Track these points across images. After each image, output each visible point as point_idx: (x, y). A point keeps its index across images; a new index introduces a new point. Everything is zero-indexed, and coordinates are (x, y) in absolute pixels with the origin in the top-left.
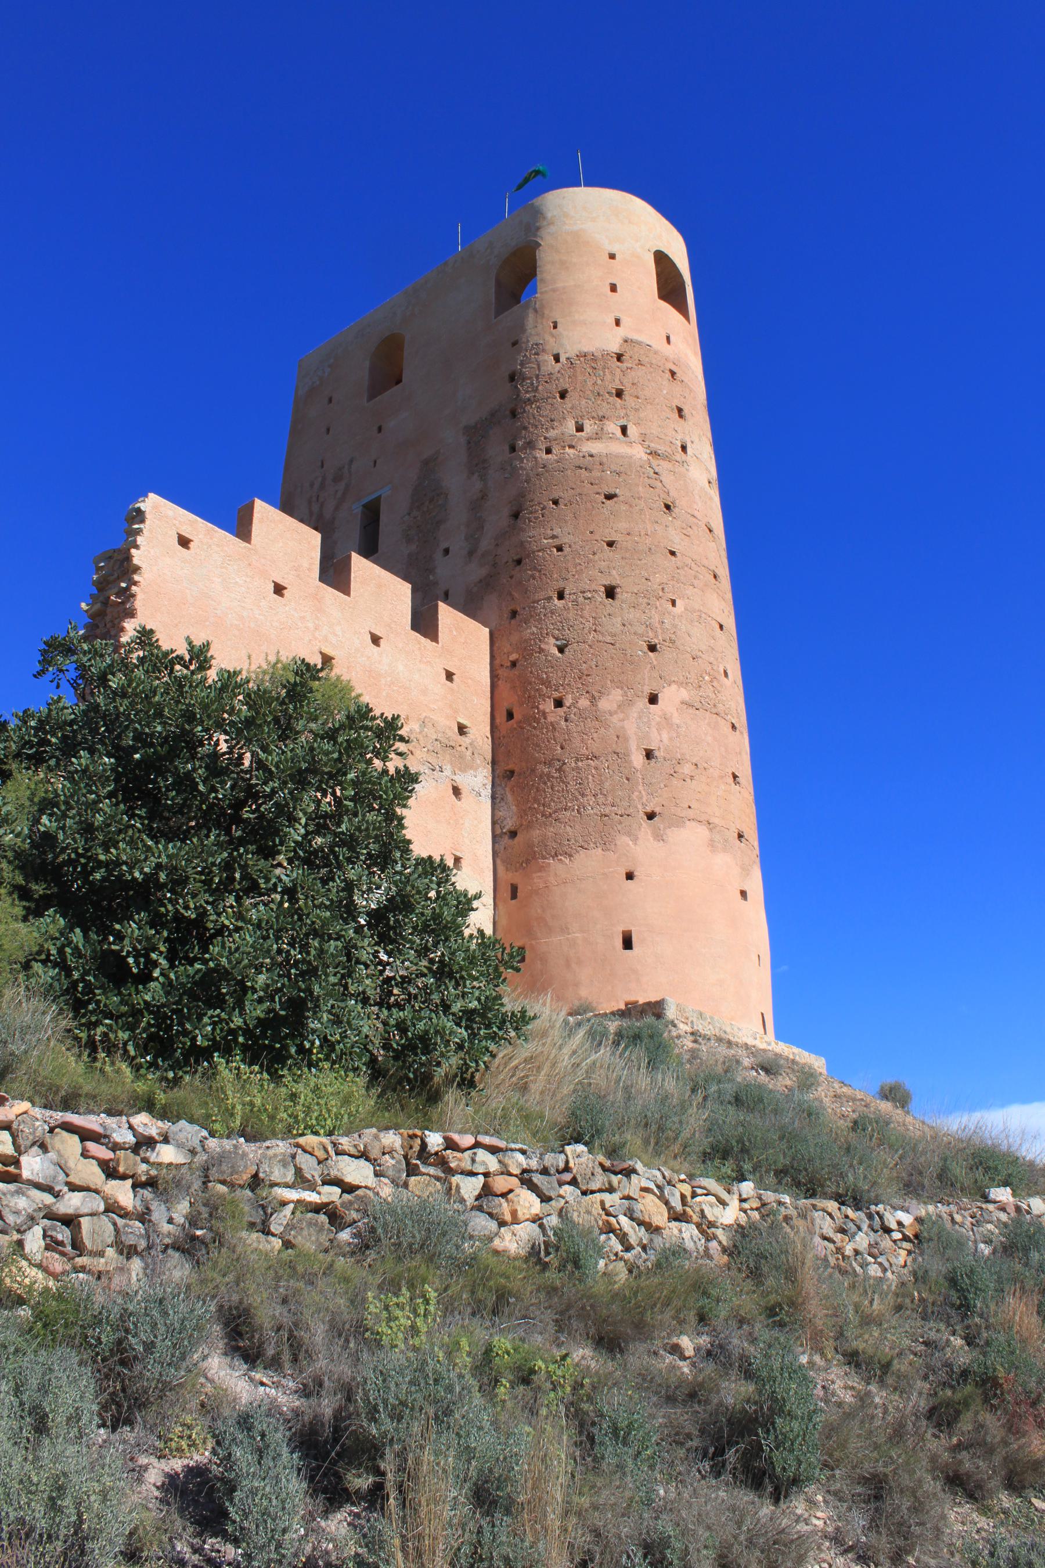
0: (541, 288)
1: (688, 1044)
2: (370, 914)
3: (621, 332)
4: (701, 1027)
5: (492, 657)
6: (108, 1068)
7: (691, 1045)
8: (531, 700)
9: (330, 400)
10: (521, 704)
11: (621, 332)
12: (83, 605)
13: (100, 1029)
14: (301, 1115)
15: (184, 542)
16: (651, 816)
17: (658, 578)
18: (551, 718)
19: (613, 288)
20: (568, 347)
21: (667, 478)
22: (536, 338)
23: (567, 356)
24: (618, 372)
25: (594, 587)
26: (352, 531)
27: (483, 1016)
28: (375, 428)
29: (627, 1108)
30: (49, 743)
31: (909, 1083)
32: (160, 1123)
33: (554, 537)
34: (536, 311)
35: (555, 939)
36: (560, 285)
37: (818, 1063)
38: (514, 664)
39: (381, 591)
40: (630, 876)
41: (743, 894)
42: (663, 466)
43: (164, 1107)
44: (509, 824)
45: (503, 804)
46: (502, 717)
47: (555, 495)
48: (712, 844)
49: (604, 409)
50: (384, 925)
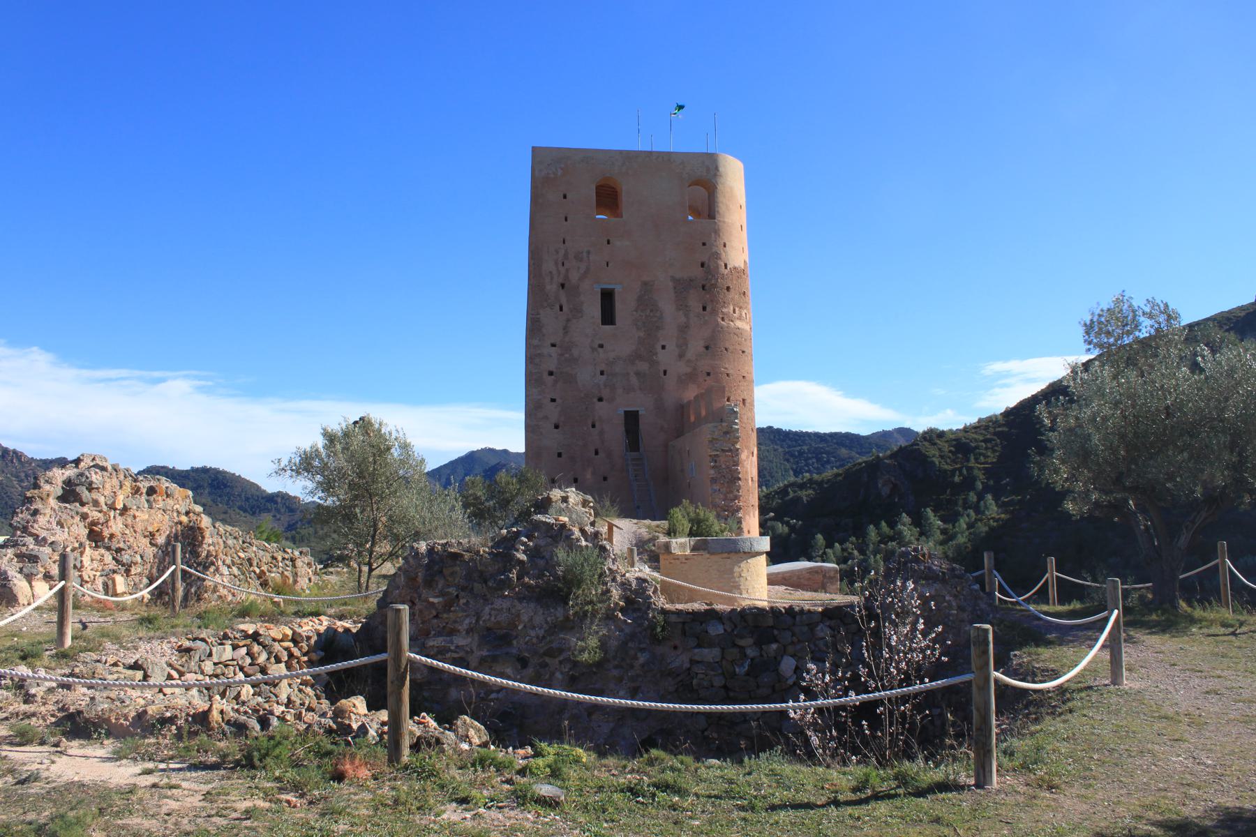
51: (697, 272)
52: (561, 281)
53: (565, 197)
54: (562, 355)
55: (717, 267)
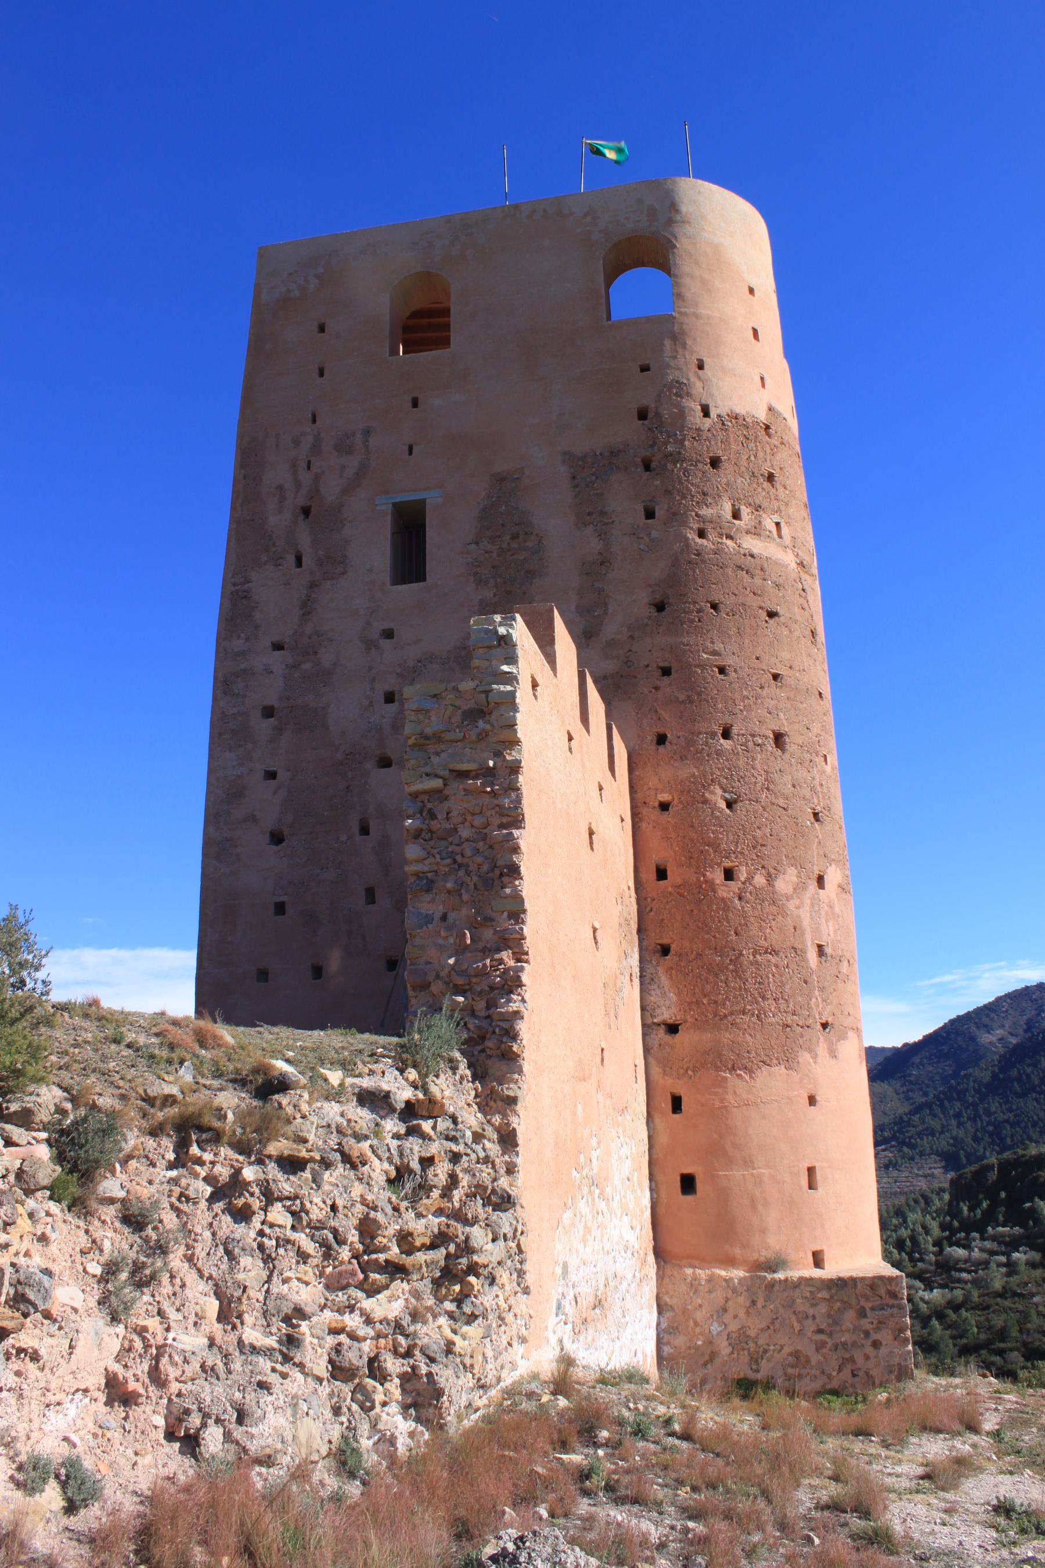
16: (825, 1026)
20: (719, 402)
22: (677, 373)
23: (718, 411)
28: (407, 399)
35: (737, 1173)
44: (666, 1014)
45: (655, 987)
47: (716, 597)
51: (627, 432)
52: (301, 501)
53: (322, 329)
54: (295, 666)
55: (682, 414)
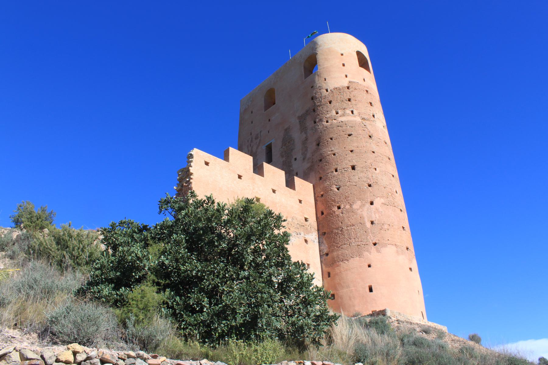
0: (319, 67)
1: (396, 324)
2: (279, 284)
3: (348, 79)
4: (401, 318)
5: (315, 194)
6: (192, 344)
7: (397, 325)
8: (329, 207)
9: (252, 112)
10: (326, 209)
11: (348, 79)
12: (175, 188)
13: (187, 330)
14: (260, 357)
15: (207, 164)
16: (375, 244)
17: (369, 161)
18: (337, 213)
19: (344, 65)
21: (369, 127)
24: (348, 93)
25: (347, 166)
26: (264, 155)
27: (322, 317)
29: (375, 348)
30: (164, 233)
31: (480, 334)
32: (211, 363)
33: (332, 151)
34: (318, 75)
35: (345, 290)
36: (325, 66)
37: (444, 329)
38: (322, 195)
39: (274, 175)
40: (369, 266)
41: (411, 269)
42: (366, 123)
43: (212, 357)
44: (325, 251)
46: (319, 214)
47: (331, 137)
48: (397, 252)
49: (345, 106)
50: (283, 288)
